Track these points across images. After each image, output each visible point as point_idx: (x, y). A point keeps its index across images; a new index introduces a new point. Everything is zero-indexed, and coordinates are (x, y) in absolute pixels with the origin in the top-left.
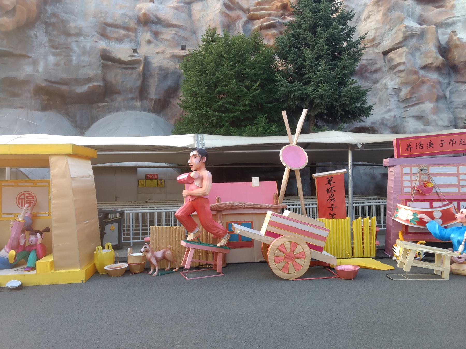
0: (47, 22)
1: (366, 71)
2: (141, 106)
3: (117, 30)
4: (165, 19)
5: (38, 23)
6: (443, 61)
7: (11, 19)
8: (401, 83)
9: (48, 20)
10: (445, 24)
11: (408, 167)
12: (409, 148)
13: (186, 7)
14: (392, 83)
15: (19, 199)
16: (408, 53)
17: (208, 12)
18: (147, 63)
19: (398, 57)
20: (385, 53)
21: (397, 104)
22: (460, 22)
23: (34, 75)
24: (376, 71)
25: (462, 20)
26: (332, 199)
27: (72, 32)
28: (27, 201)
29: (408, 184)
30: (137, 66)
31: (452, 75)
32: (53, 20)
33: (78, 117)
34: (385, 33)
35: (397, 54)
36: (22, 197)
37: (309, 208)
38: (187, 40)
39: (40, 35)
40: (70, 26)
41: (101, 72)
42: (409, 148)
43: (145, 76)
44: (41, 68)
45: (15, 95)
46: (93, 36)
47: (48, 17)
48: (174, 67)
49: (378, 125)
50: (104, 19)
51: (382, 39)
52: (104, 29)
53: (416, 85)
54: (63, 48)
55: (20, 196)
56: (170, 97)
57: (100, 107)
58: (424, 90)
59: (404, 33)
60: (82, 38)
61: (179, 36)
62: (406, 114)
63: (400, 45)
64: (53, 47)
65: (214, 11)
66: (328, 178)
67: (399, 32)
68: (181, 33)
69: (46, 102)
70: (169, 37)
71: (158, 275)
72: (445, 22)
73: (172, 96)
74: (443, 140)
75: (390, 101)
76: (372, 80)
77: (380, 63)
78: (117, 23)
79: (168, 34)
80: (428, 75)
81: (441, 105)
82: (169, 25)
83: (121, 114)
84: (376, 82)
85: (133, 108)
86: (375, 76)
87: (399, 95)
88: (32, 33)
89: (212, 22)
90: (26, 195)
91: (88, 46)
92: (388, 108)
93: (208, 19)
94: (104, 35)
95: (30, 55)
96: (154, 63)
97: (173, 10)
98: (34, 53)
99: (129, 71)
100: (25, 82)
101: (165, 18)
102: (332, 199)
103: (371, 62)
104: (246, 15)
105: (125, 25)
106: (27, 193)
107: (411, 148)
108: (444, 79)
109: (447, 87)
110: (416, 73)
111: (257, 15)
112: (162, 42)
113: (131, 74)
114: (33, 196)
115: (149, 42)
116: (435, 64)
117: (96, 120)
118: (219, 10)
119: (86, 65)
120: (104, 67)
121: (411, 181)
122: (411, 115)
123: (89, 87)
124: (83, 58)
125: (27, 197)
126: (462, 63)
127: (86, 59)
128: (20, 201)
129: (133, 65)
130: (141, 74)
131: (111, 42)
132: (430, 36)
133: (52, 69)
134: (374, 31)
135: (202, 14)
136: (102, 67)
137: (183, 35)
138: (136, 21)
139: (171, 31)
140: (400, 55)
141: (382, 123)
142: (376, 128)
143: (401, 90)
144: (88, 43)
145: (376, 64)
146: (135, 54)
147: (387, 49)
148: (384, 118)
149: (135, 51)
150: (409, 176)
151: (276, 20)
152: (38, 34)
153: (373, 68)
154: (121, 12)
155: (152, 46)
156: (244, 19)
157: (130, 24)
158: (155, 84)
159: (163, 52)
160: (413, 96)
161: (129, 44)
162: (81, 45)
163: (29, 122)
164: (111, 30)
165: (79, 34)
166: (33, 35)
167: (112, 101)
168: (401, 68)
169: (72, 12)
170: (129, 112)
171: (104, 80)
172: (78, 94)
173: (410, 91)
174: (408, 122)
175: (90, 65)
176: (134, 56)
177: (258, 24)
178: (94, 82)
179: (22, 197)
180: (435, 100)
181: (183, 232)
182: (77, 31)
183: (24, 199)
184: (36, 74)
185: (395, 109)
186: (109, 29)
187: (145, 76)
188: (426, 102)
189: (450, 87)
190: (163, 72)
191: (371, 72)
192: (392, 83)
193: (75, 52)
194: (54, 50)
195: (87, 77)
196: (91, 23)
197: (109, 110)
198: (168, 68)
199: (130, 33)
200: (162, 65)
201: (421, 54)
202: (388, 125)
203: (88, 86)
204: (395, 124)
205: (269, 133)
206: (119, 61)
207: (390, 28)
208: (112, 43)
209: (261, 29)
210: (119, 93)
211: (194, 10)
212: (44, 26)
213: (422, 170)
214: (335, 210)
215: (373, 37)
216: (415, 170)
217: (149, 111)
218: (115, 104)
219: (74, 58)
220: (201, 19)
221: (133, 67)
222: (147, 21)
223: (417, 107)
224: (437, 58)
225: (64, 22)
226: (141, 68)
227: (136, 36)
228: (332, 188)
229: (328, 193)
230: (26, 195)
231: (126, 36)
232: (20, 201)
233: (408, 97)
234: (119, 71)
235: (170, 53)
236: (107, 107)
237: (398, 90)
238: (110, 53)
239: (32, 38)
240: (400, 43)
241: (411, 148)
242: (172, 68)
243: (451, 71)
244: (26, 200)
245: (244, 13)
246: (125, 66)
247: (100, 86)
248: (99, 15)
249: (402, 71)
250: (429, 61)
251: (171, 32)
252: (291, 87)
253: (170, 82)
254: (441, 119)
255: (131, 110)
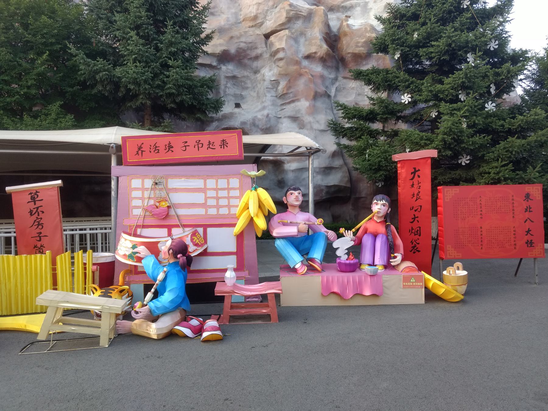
1: (245, 57)
6: (328, 51)
8: (279, 74)
10: (343, 7)
11: (137, 178)
12: (140, 152)
14: (270, 74)
16: (289, 37)
19: (279, 42)
20: (267, 36)
21: (273, 101)
22: (359, 6)
24: (257, 58)
25: (362, 4)
26: (39, 225)
29: (139, 203)
31: (341, 69)
34: (267, 10)
35: (278, 38)
42: (140, 152)
49: (248, 126)
51: (265, 17)
53: (292, 78)
58: (301, 84)
59: (288, 12)
62: (281, 114)
63: (283, 27)
66: (31, 194)
67: (282, 10)
72: (343, 4)
74: (186, 142)
75: (266, 96)
76: (252, 69)
77: (261, 49)
80: (312, 66)
81: (320, 104)
84: (256, 72)
86: (255, 64)
87: (277, 89)
92: (263, 104)
102: (39, 225)
103: (250, 45)
107: (142, 151)
108: (330, 74)
109: (333, 84)
110: (298, 63)
116: (319, 54)
121: (142, 199)
122: (287, 115)
126: (349, 55)
132: (318, 20)
134: (255, 7)
140: (281, 39)
141: (253, 123)
142: (246, 130)
143: (279, 83)
145: (256, 48)
147: (269, 31)
148: (256, 117)
150: (140, 192)
153: (253, 54)
160: (290, 91)
168: (281, 55)
173: (287, 84)
174: (282, 124)
180: (311, 97)
185: (270, 107)
188: (302, 100)
189: (337, 84)
191: (251, 59)
192: (270, 74)
201: (306, 40)
202: (260, 127)
204: (268, 126)
207: (274, 5)
213: (156, 184)
214: (44, 241)
215: (255, 14)
216: (149, 183)
223: (292, 105)
224: (321, 47)
228: (38, 208)
229: (31, 215)
233: (285, 92)
237: (276, 83)
240: (283, 24)
241: (142, 151)
243: (340, 65)
249: (281, 59)
250: (313, 49)
254: (318, 122)
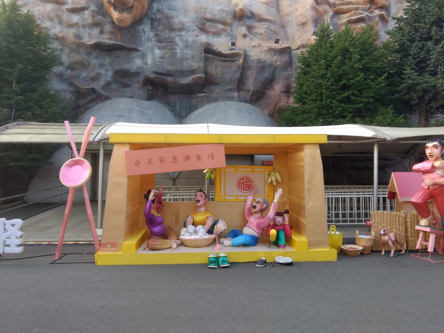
0: (152, 18)
2: (238, 97)
3: (215, 24)
4: (258, 14)
5: (145, 19)
7: (130, 15)
9: (154, 17)
13: (274, 2)
15: (239, 183)
17: (298, 6)
18: (246, 56)
23: (143, 67)
27: (176, 27)
28: (246, 185)
30: (235, 58)
32: (159, 16)
33: (178, 106)
36: (242, 181)
37: (332, 198)
38: (277, 34)
39: (146, 30)
40: (174, 22)
41: (202, 64)
43: (244, 68)
44: (149, 60)
45: (126, 86)
46: (194, 30)
47: (154, 14)
48: (270, 60)
50: (204, 14)
52: (204, 24)
54: (167, 42)
55: (240, 181)
56: (266, 89)
57: (200, 97)
60: (184, 32)
61: (271, 30)
64: (159, 41)
65: (305, 6)
68: (272, 27)
69: (150, 92)
70: (262, 31)
71: (394, 257)
73: (267, 87)
78: (216, 18)
79: (261, 28)
82: (262, 20)
83: (221, 105)
85: (231, 99)
88: (140, 28)
89: (303, 17)
90: (245, 179)
91: (190, 40)
93: (299, 14)
94: (203, 30)
95: (139, 49)
96: (252, 56)
97: (264, 5)
98: (143, 47)
99: (228, 64)
100: (136, 74)
101: (259, 13)
104: (332, 9)
105: (223, 20)
106: (246, 178)
111: (343, 9)
112: (255, 36)
113: (231, 66)
114: (251, 181)
115: (245, 36)
117: (194, 109)
118: (311, 5)
119: (189, 57)
120: (206, 59)
123: (193, 79)
124: (186, 51)
125: (246, 181)
127: (188, 52)
128: (240, 184)
129: (232, 58)
130: (241, 66)
131: (208, 36)
133: (159, 62)
135: (291, 8)
136: (204, 59)
137: (274, 29)
138: (232, 16)
139: (263, 25)
144: (190, 37)
146: (234, 47)
149: (233, 44)
151: (363, 14)
152: (145, 29)
154: (219, 8)
155: (248, 39)
156: (331, 13)
157: (227, 19)
158: (254, 76)
159: (260, 45)
161: (226, 37)
162: (184, 39)
163: (142, 111)
164: (209, 25)
165: (181, 29)
166: (141, 30)
167: (211, 91)
169: (174, 9)
170: (227, 102)
171: (206, 72)
172: (182, 85)
175: (193, 57)
176: (233, 49)
177: (344, 18)
178: (196, 74)
179: (242, 181)
181: (403, 217)
182: (180, 26)
183: (244, 183)
184: (145, 66)
186: (208, 23)
187: (244, 68)
190: (261, 64)
193: (178, 46)
194: (159, 44)
195: (191, 69)
196: (192, 18)
197: (210, 100)
198: (265, 61)
199: (227, 27)
200: (260, 57)
203: (192, 77)
205: (396, 123)
206: (219, 54)
208: (210, 36)
209: (349, 23)
210: (217, 84)
211: (283, 5)
212: (150, 22)
217: (245, 101)
218: (214, 95)
219: (178, 51)
220: (290, 14)
221: (232, 59)
222: (242, 16)
225: (168, 18)
226: (241, 61)
227: (231, 30)
230: (245, 179)
231: (223, 30)
232: (240, 184)
234: (219, 63)
235: (267, 47)
236: (206, 98)
238: (211, 46)
239: (140, 32)
242: (269, 61)
244: (245, 184)
245: (330, 8)
246: (224, 59)
247: (202, 77)
248: (200, 11)
251: (263, 26)
252: (419, 80)
253: (266, 74)
255: (229, 101)
